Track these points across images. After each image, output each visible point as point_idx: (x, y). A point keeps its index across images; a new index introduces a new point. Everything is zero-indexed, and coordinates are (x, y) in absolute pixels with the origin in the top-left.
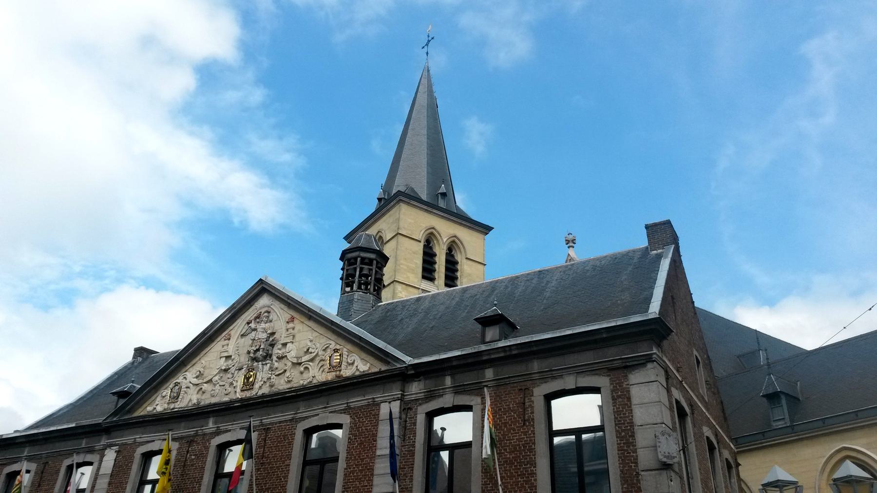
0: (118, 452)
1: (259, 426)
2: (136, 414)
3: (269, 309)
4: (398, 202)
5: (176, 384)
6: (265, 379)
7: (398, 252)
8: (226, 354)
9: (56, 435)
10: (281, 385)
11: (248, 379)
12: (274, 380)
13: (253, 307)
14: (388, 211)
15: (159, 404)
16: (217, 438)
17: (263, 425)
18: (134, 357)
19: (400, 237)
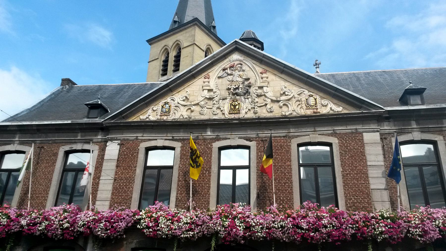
0: (121, 145)
1: (256, 138)
2: (130, 120)
3: (241, 63)
4: (194, 25)
5: (166, 103)
6: (250, 108)
7: (194, 54)
8: (208, 88)
9: (67, 127)
10: (263, 113)
11: (235, 106)
12: (258, 110)
13: (227, 60)
14: (181, 31)
15: (151, 114)
16: (217, 142)
17: (259, 137)
18: (62, 85)
19: (195, 46)
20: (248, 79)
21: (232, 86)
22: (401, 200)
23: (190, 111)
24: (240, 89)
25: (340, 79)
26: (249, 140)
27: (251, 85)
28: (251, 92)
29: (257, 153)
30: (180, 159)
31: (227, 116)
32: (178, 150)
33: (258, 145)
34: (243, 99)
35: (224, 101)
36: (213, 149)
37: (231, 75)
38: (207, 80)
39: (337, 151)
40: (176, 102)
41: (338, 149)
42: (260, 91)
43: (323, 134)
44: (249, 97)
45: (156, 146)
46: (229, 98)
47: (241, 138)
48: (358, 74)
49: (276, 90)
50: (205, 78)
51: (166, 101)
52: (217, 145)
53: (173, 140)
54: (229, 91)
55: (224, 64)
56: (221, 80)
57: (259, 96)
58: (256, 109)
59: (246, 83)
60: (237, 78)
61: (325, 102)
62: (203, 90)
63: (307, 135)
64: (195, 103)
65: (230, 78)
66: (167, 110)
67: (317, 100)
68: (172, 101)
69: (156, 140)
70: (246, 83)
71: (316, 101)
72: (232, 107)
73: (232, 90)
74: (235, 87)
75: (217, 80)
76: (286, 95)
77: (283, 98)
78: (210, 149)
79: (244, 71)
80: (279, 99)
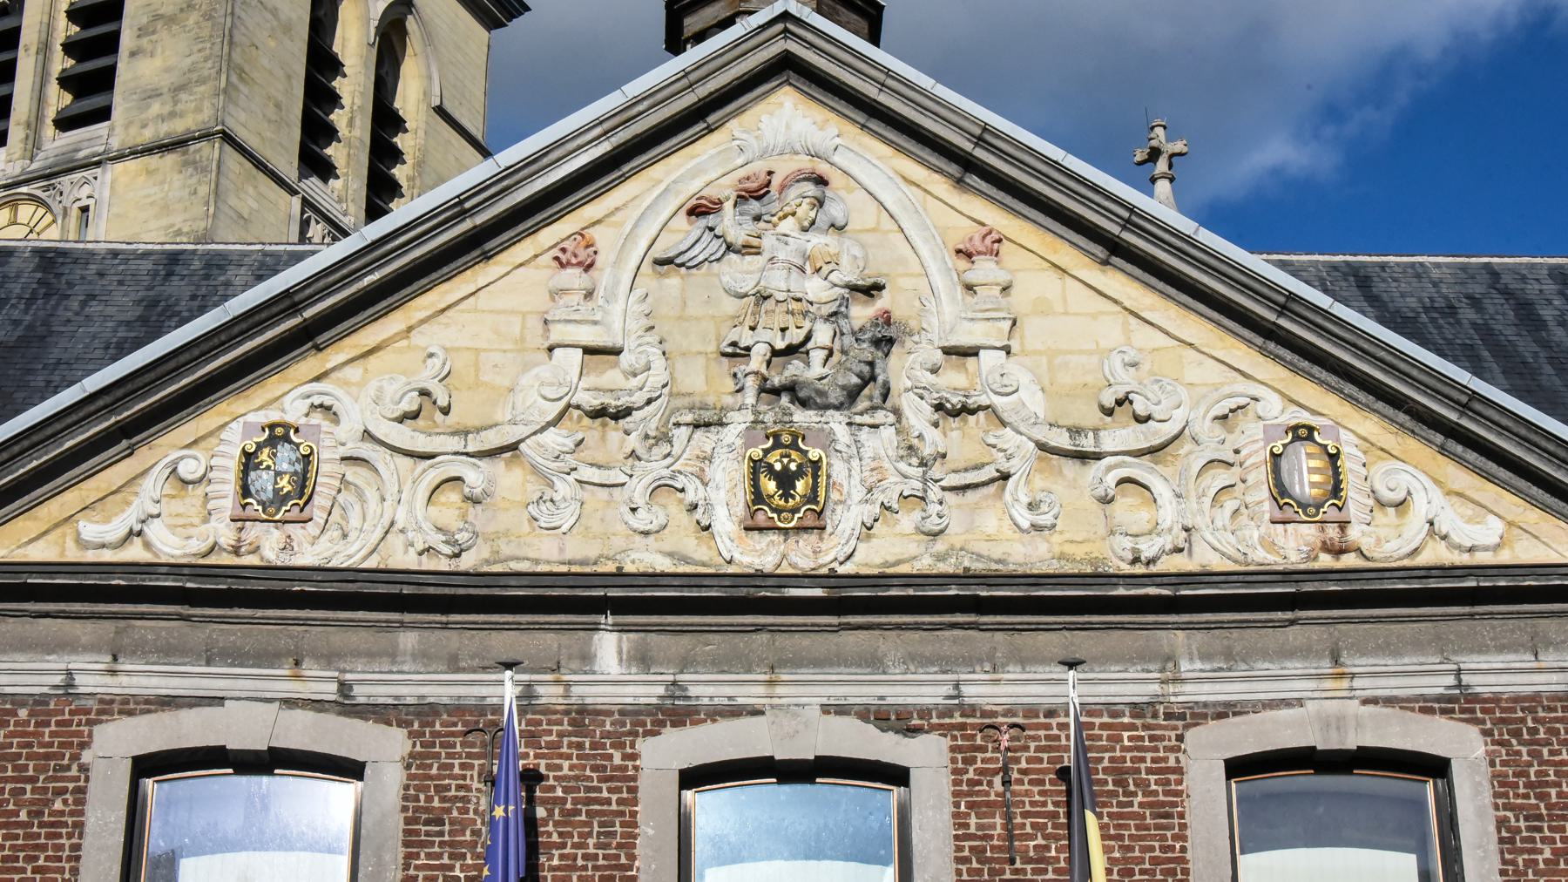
3: (823, 168)
5: (278, 435)
6: (892, 499)
16: (670, 735)
21: (763, 334)
23: (452, 496)
24: (817, 356)
25: (1412, 302)
26: (901, 721)
27: (891, 332)
28: (899, 383)
29: (959, 820)
30: (401, 851)
31: (727, 547)
32: (389, 778)
33: (964, 755)
34: (842, 433)
36: (642, 783)
37: (749, 249)
38: (573, 277)
39: (1480, 813)
40: (348, 429)
41: (1487, 798)
43: (1390, 701)
44: (880, 416)
45: (1312, 749)
46: (739, 422)
47: (841, 710)
48: (1521, 275)
51: (274, 416)
52: (666, 753)
53: (346, 706)
54: (741, 368)
55: (694, 173)
56: (674, 281)
57: (951, 411)
59: (861, 313)
60: (793, 266)
61: (1394, 478)
62: (551, 349)
63: (1286, 703)
64: (492, 439)
65: (740, 273)
66: (285, 484)
67: (1345, 464)
68: (317, 418)
69: (218, 701)
70: (861, 313)
71: (1336, 472)
72: (770, 486)
73: (757, 362)
76: (1142, 420)
77: (1120, 436)
78: (626, 780)
80: (1087, 444)
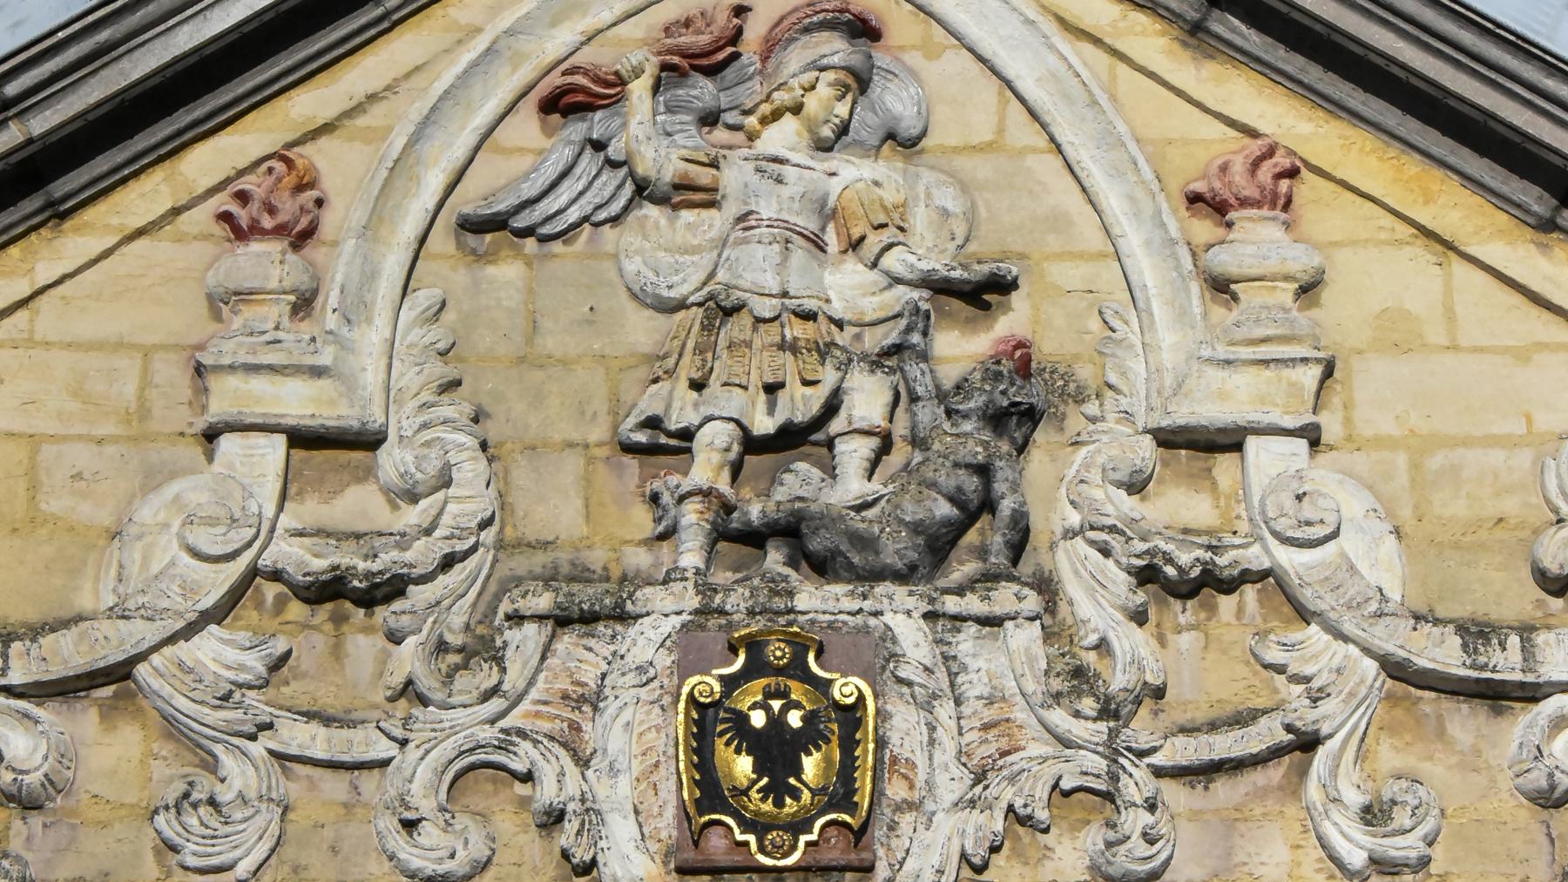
8: (300, 402)
20: (983, 293)
22: (692, 293)
24: (854, 452)
28: (1053, 515)
35: (581, 657)
38: (264, 262)
42: (1180, 509)
44: (1004, 598)
49: (1453, 507)
50: (241, 234)
54: (670, 482)
56: (507, 273)
58: (1135, 821)
59: (959, 348)
62: (211, 436)
64: (68, 654)
70: (959, 348)
74: (764, 425)
75: (446, 270)
79: (902, 142)
80: (1506, 663)
